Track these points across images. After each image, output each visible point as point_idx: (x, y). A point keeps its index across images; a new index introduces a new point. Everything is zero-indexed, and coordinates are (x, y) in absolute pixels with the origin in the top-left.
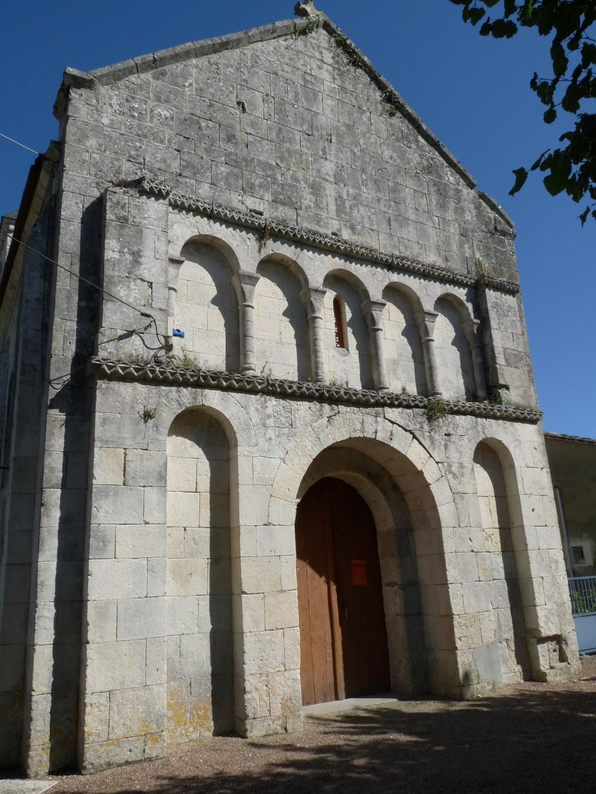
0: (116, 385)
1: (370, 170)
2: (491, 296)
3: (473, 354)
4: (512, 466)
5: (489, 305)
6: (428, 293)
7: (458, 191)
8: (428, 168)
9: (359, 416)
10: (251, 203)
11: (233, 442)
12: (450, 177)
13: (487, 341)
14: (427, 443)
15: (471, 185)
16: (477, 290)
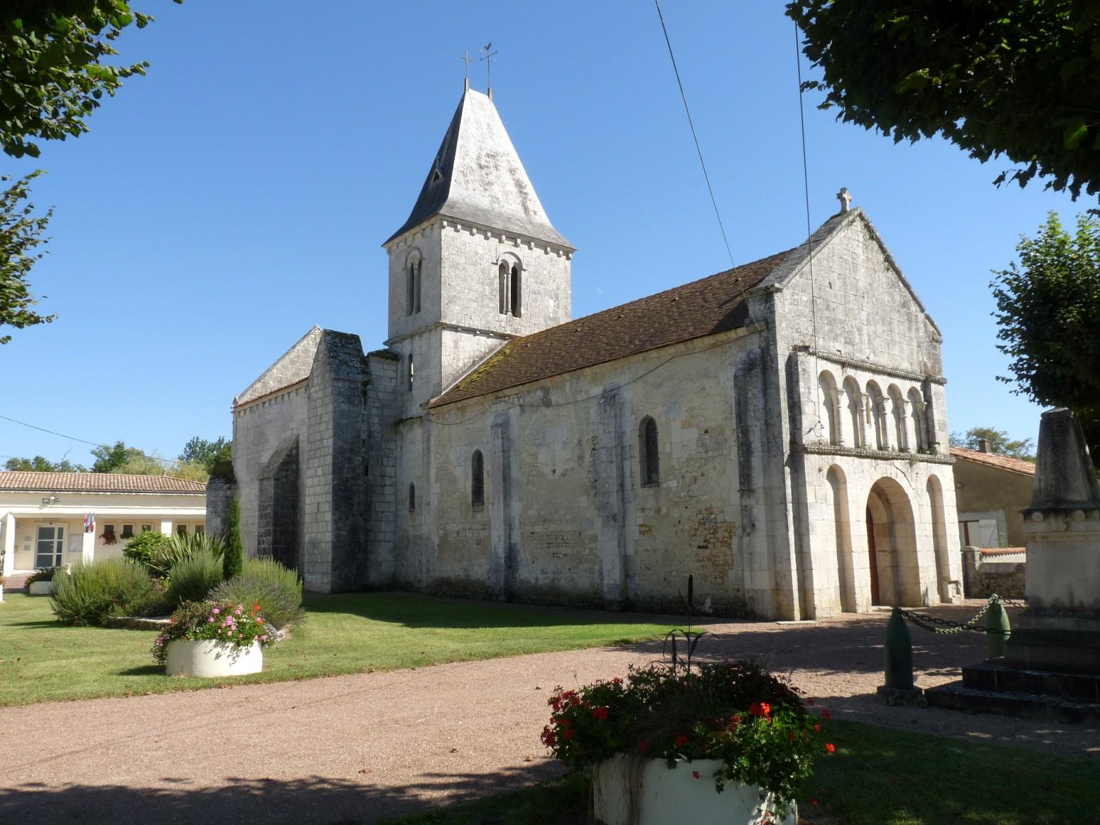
0: (810, 456)
1: (880, 313)
2: (933, 386)
3: (921, 423)
4: (940, 490)
5: (933, 393)
6: (904, 386)
7: (917, 316)
8: (904, 303)
9: (884, 465)
10: (839, 346)
11: (842, 481)
12: (914, 308)
13: (930, 415)
14: (910, 479)
15: (922, 311)
16: (926, 384)
